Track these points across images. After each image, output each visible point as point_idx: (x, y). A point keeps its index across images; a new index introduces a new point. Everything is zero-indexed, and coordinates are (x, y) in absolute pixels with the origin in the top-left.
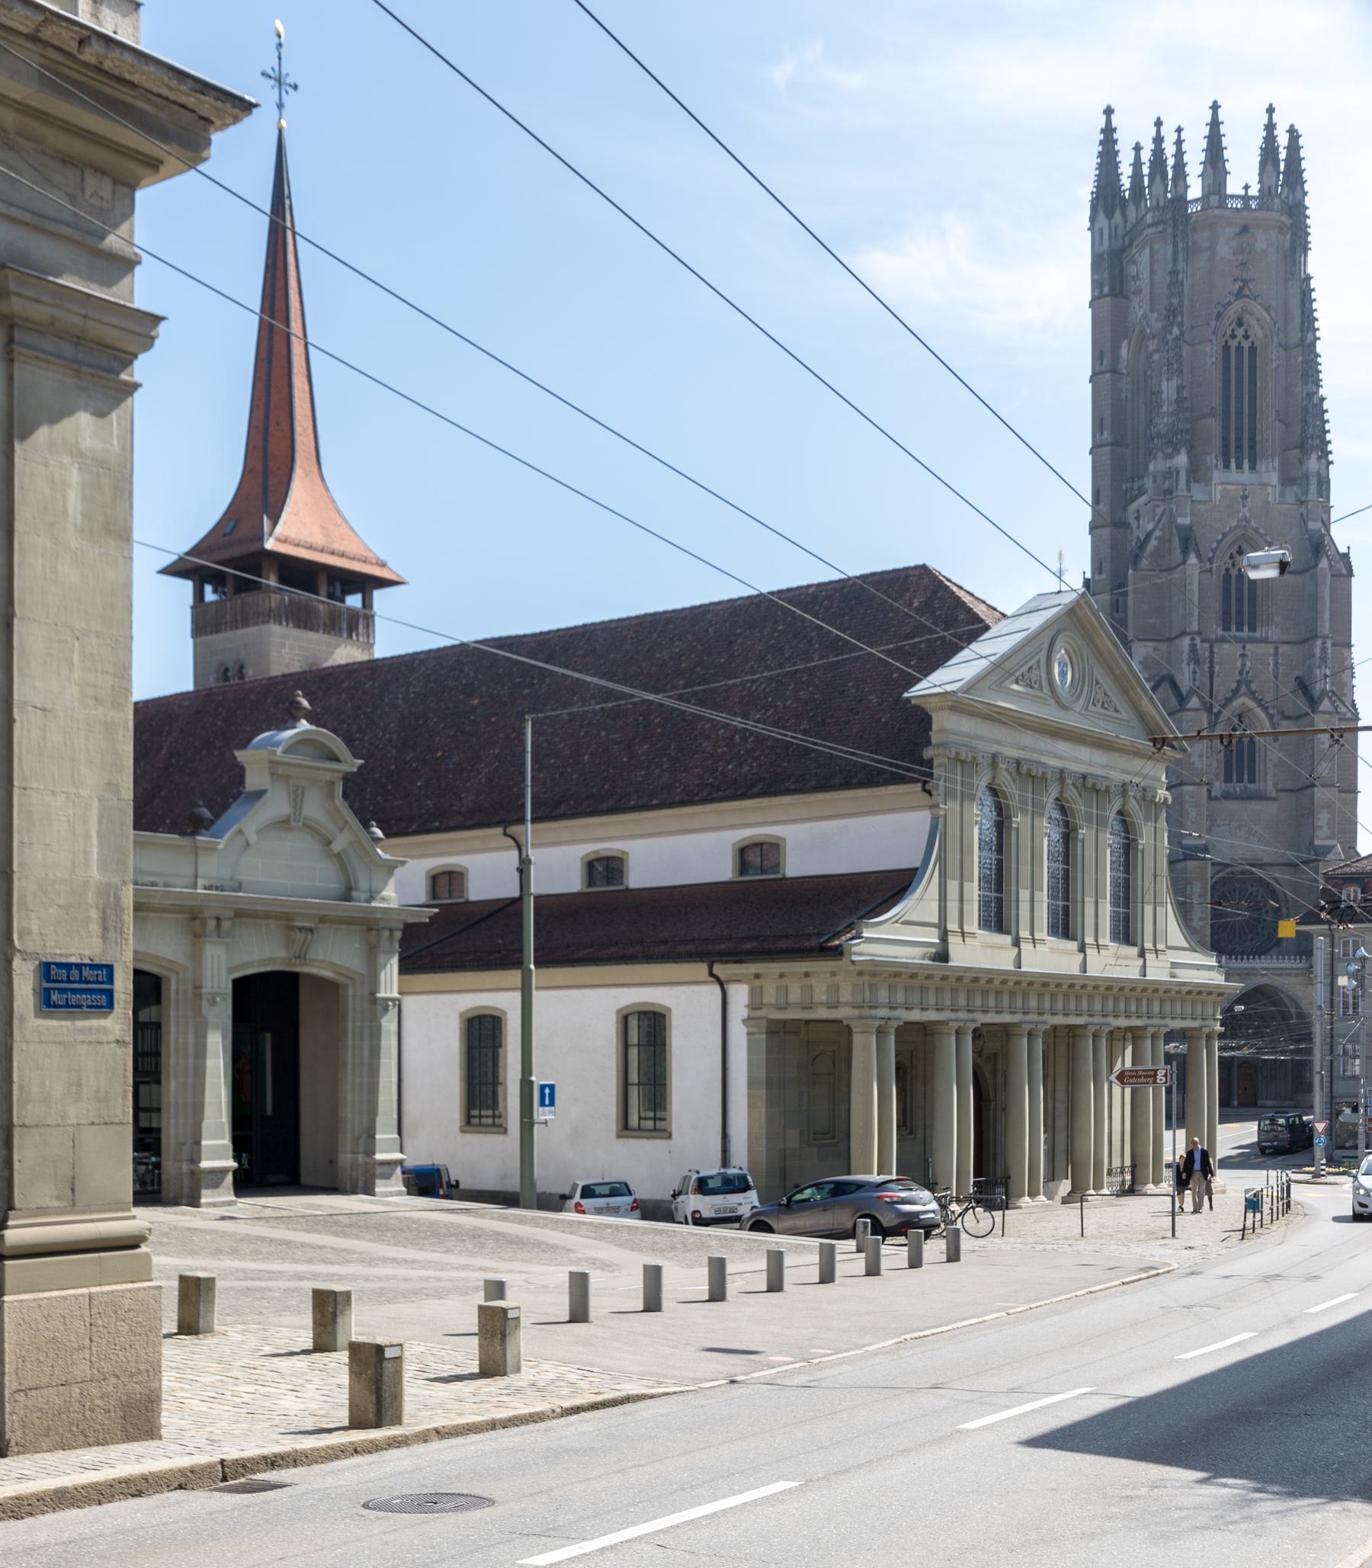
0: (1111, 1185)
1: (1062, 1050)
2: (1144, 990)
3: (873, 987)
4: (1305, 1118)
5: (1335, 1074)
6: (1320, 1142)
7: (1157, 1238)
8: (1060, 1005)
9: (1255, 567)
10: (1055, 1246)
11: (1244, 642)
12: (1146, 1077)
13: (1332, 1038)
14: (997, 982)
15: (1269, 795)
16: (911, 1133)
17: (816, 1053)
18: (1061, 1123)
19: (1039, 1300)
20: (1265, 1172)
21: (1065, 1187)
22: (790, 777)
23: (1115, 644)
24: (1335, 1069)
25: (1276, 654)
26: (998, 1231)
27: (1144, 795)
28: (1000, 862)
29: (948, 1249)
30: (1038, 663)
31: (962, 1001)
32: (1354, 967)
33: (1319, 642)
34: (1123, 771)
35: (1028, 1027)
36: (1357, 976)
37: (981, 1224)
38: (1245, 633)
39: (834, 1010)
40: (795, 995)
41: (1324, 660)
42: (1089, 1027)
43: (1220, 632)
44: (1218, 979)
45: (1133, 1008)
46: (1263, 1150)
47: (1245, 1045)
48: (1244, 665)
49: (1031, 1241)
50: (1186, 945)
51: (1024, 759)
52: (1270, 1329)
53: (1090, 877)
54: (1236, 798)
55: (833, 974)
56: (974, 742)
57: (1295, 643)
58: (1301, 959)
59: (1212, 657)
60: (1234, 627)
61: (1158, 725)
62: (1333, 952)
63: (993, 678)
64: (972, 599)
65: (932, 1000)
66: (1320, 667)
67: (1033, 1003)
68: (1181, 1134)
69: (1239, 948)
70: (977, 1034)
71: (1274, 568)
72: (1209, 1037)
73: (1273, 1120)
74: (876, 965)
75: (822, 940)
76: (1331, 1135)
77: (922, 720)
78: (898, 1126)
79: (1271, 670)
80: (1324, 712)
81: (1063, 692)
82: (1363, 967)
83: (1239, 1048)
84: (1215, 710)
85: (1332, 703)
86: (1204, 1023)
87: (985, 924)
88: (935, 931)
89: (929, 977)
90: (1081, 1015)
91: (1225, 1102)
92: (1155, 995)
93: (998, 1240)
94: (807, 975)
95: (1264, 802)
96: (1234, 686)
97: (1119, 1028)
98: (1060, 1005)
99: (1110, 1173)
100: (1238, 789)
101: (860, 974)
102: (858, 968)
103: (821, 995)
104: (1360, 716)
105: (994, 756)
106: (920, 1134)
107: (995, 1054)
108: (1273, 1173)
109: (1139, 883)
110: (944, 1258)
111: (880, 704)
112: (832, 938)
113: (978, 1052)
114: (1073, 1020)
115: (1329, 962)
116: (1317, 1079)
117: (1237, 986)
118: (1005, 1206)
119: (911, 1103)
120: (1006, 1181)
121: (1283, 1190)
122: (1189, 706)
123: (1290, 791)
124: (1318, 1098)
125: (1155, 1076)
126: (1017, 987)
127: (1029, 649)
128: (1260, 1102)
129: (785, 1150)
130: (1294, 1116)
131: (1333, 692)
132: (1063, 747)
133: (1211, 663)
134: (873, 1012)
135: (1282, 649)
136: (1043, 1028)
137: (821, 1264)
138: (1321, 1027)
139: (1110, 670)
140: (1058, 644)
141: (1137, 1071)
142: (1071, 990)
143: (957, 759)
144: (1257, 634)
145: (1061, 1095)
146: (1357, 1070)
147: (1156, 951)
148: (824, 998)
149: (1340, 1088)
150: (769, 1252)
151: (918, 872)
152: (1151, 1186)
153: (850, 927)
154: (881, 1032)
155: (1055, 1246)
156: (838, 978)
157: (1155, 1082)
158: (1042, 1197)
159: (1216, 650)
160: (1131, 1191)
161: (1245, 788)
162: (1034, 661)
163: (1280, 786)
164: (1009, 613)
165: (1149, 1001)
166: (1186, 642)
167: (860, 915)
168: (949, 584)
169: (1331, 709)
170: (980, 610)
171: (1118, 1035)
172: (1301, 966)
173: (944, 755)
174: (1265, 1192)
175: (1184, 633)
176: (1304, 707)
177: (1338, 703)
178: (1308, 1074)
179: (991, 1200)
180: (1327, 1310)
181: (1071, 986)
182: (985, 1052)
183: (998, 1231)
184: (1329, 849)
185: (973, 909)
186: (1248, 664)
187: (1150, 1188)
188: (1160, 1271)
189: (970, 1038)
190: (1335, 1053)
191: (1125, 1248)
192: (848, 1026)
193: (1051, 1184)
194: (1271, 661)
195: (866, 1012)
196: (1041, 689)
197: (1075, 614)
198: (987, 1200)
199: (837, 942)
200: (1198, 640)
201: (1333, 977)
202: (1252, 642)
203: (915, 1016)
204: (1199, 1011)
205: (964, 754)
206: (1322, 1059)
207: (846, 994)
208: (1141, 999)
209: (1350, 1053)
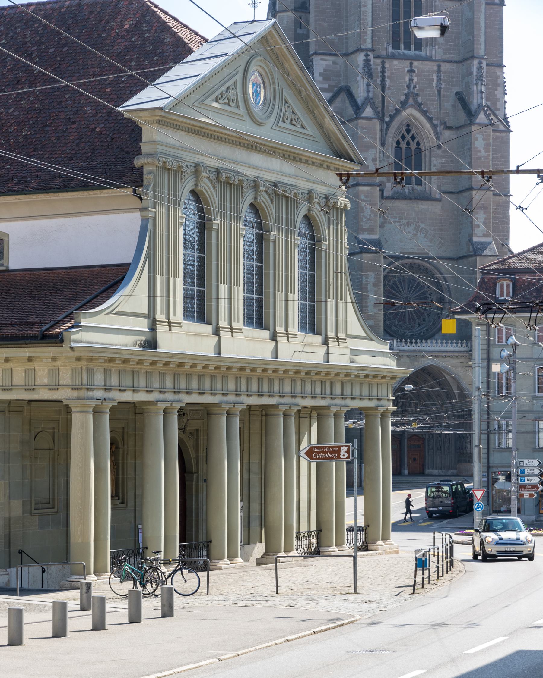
0: (299, 547)
1: (256, 426)
2: (328, 374)
3: (90, 371)
4: (466, 486)
5: (491, 446)
6: (479, 508)
7: (341, 594)
8: (255, 387)
9: (420, 28)
10: (255, 602)
11: (412, 59)
12: (331, 452)
13: (488, 414)
14: (199, 367)
15: (433, 196)
16: (123, 503)
17: (38, 431)
18: (255, 492)
19: (244, 648)
20: (431, 534)
21: (259, 549)
22: (12, 179)
23: (301, 68)
24: (491, 442)
25: (439, 71)
26: (203, 589)
27: (327, 202)
28: (202, 260)
29: (163, 606)
30: (235, 83)
31: (169, 384)
32: (506, 353)
33: (476, 62)
34: (309, 181)
35: (226, 407)
36: (511, 360)
37: (187, 585)
38: (412, 52)
39: (56, 392)
40: (19, 378)
41: (480, 78)
42: (280, 407)
43: (390, 49)
44: (391, 364)
45: (318, 390)
46: (430, 515)
47: (414, 421)
48: (411, 80)
49: (232, 598)
50: (364, 334)
51: (223, 169)
52: (436, 667)
53: (281, 273)
54: (405, 199)
55: (54, 359)
56: (180, 153)
57: (455, 62)
58: (462, 343)
59: (383, 72)
60: (402, 46)
61: (339, 140)
62: (489, 340)
63: (195, 96)
64: (176, 23)
65: (142, 383)
66: (476, 84)
67: (231, 386)
68: (361, 499)
69: (408, 333)
70: (182, 413)
71: (437, 29)
72: (384, 415)
73: (438, 487)
74: (93, 352)
75: (44, 328)
76: (488, 501)
77: (133, 130)
78: (112, 497)
79: (434, 85)
80: (479, 124)
81: (257, 110)
82: (514, 352)
83: (409, 423)
84: (387, 119)
85: (487, 116)
86: (379, 403)
87: (189, 314)
88: (145, 321)
89: (140, 362)
90: (273, 396)
91: (397, 472)
92: (337, 378)
93: (204, 598)
94: (30, 359)
95: (429, 203)
96: (403, 98)
97: (306, 407)
98: (255, 387)
99: (298, 537)
100: (407, 191)
101: (79, 359)
102: (77, 354)
103: (43, 378)
104: (511, 128)
105: (197, 166)
106: (131, 504)
107: (197, 430)
108: (438, 536)
109: (323, 279)
110: (159, 613)
111: (94, 115)
112: (53, 327)
113: (182, 430)
114: (266, 401)
115: (485, 347)
116: (476, 451)
117: (407, 371)
118: (206, 568)
119: (123, 474)
120: (207, 545)
121: (447, 549)
122: (364, 115)
123: (451, 193)
124: (477, 468)
125: (339, 452)
126: (217, 371)
127: (227, 71)
128: (427, 471)
129: (9, 518)
130: (457, 484)
131: (488, 106)
132: (257, 159)
133: (383, 77)
134: (90, 394)
135: (445, 67)
136: (240, 407)
137: (54, 620)
138: (479, 406)
139: (297, 92)
140: (253, 68)
141: (323, 447)
142: (265, 374)
143: (164, 168)
144: (423, 53)
145: (255, 467)
146: (510, 443)
147: (338, 339)
148: (46, 381)
149: (496, 459)
150: (9, 610)
151: (130, 268)
152: (334, 548)
153: (70, 316)
154: (97, 411)
155: (255, 602)
156: (58, 363)
157: (339, 457)
158: (239, 559)
159: (387, 65)
160: (317, 553)
161: (413, 189)
162: (231, 82)
163: (443, 189)
164: (210, 39)
165: (332, 383)
166: (361, 57)
167: (78, 306)
168: (156, 10)
169: (486, 121)
170: (183, 34)
171: (305, 413)
172: (462, 349)
173: (153, 164)
174: (432, 553)
175: (359, 50)
176: (462, 117)
177: (492, 117)
178: (468, 446)
179: (195, 562)
180: (483, 651)
181: (265, 370)
182: (188, 428)
183: (203, 589)
184: (486, 245)
185: (178, 304)
186: (415, 79)
187: (334, 550)
188: (345, 622)
189: (176, 417)
190: (491, 428)
191: (315, 603)
192: (67, 406)
193: (246, 547)
194: (435, 77)
195: (84, 393)
196: (238, 107)
197: (267, 42)
198: (191, 562)
199: (58, 331)
200: (371, 57)
201: (489, 360)
202: (419, 60)
203: (128, 396)
204: (375, 393)
205: (171, 163)
206: (480, 433)
207: (66, 377)
208: (325, 382)
209: (504, 427)
